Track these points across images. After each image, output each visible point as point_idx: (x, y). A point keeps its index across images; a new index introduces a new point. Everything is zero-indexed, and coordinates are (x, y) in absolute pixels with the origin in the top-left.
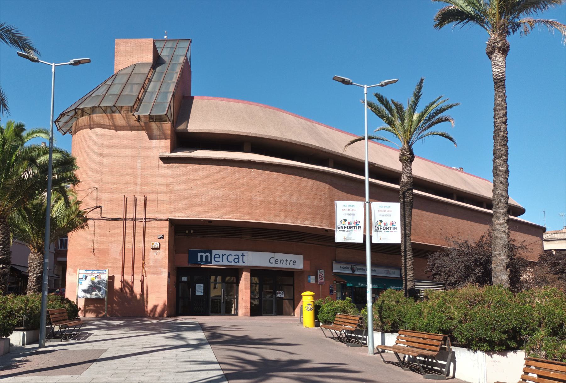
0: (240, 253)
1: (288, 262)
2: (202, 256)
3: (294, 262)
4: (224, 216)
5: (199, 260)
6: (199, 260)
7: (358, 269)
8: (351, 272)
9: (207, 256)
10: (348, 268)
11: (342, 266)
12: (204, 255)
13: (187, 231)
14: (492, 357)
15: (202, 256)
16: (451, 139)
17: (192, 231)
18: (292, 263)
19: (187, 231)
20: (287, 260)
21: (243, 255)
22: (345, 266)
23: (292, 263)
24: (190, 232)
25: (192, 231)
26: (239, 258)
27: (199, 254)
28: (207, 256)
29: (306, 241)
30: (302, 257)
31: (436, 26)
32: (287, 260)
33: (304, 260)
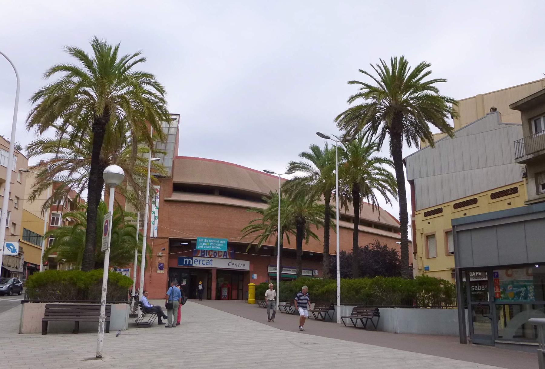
2: (186, 261)
3: (244, 265)
12: (188, 260)
15: (186, 261)
27: (185, 260)
28: (190, 261)
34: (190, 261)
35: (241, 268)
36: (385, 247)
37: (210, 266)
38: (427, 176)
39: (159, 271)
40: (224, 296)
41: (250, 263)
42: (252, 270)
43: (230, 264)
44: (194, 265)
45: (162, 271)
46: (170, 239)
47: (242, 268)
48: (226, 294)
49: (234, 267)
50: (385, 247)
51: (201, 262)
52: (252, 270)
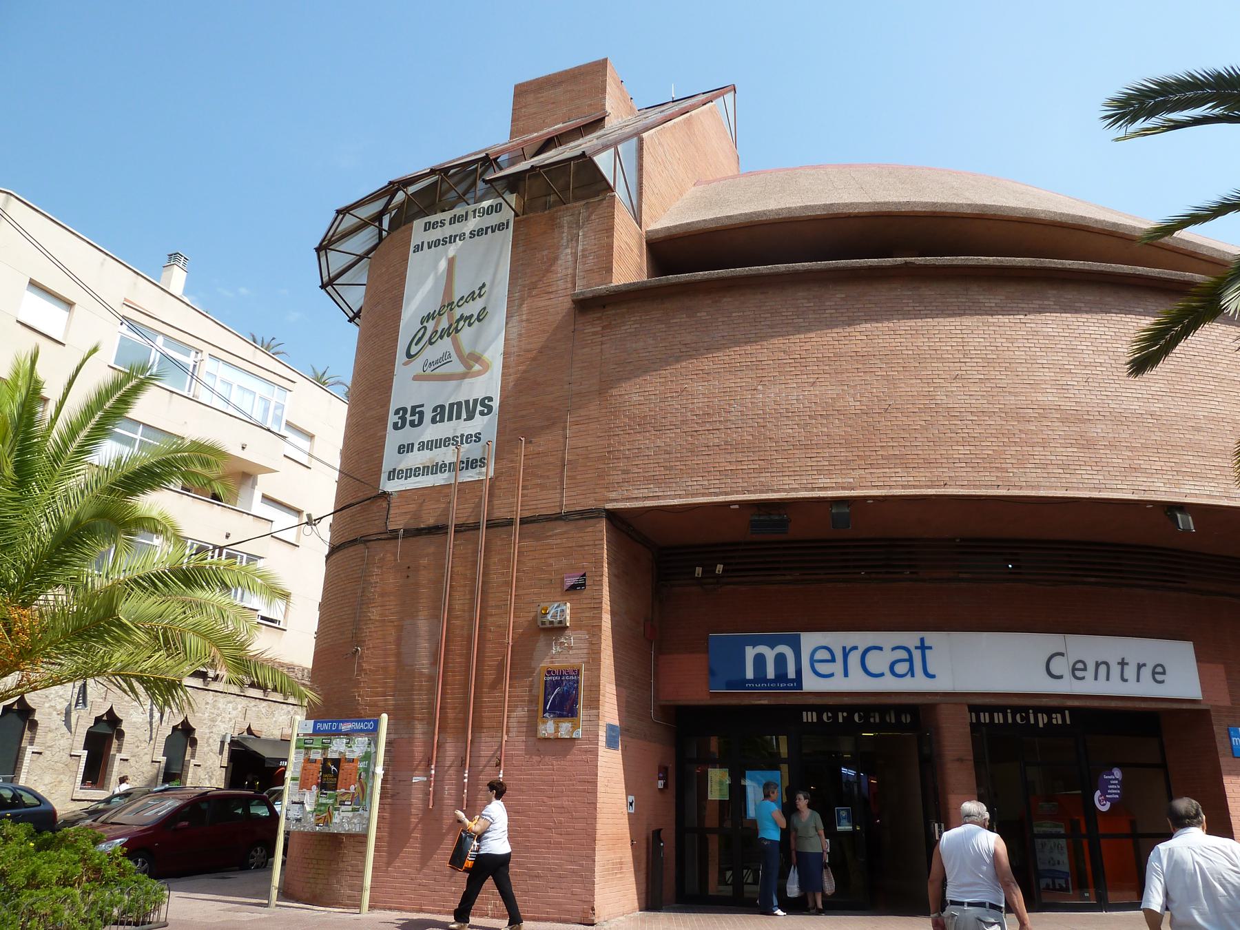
0: (910, 639)
1: (1130, 672)
2: (760, 660)
3: (1159, 672)
5: (750, 674)
6: (750, 674)
12: (770, 654)
15: (760, 660)
18: (1146, 673)
20: (1123, 663)
21: (923, 647)
23: (1146, 673)
24: (709, 571)
26: (910, 660)
27: (750, 653)
28: (780, 660)
34: (780, 660)
35: (1144, 688)
36: (423, 733)
37: (917, 684)
38: (302, 803)
39: (548, 728)
40: (1054, 875)
41: (1201, 658)
42: (1225, 701)
43: (1059, 666)
44: (811, 684)
45: (565, 729)
46: (624, 525)
47: (1145, 688)
48: (1063, 862)
49: (1090, 686)
50: (423, 733)
51: (854, 658)
52: (1225, 701)
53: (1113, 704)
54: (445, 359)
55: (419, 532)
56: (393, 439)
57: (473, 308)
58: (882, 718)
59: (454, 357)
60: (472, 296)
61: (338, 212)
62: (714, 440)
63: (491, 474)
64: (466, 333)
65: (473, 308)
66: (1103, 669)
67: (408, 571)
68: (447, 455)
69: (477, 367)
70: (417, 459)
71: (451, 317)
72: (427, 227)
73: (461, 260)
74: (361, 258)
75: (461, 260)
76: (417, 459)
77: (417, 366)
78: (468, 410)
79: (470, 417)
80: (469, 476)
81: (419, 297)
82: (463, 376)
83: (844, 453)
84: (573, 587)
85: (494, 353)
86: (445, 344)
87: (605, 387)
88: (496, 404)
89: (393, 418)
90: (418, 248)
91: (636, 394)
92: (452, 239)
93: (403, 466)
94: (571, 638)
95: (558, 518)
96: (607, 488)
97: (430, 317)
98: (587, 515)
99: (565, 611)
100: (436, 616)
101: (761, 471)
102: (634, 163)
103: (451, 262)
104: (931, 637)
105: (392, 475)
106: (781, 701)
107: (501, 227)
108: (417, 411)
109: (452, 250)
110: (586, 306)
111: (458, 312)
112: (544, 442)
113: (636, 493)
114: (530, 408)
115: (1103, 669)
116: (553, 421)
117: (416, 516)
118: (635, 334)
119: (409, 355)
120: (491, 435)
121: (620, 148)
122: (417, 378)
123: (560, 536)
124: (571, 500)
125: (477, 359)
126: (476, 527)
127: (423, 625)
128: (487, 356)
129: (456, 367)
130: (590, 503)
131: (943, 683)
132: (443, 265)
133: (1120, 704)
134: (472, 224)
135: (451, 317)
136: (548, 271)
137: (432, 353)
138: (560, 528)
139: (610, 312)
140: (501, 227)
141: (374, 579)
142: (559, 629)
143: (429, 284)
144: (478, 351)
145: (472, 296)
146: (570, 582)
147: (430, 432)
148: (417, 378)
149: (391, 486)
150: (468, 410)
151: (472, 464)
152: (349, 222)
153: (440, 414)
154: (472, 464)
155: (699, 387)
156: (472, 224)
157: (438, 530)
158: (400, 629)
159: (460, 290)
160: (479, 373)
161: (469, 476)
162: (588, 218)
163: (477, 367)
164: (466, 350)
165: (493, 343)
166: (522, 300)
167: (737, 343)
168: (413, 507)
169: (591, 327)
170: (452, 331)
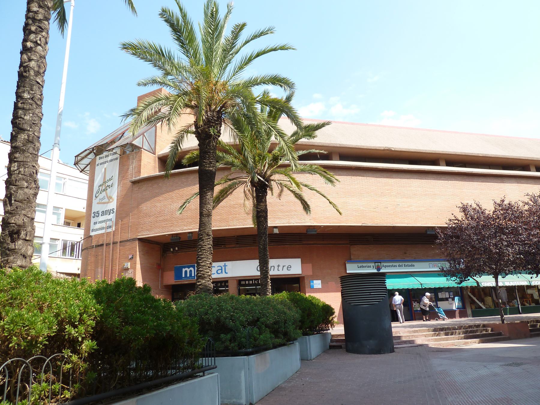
0: (222, 264)
1: (280, 268)
2: (186, 272)
3: (289, 267)
4: (185, 228)
5: (183, 276)
6: (183, 276)
7: (385, 267)
8: (375, 271)
9: (191, 271)
10: (369, 267)
11: (360, 265)
12: (188, 270)
13: (172, 249)
14: (464, 209)
15: (186, 272)
16: (282, 48)
17: (177, 248)
18: (285, 268)
19: (172, 249)
20: (279, 266)
21: (225, 266)
22: (364, 265)
23: (285, 268)
24: (174, 249)
25: (177, 248)
26: (222, 269)
27: (184, 270)
28: (191, 271)
29: (304, 242)
30: (299, 261)
31: (164, 11)
32: (279, 266)
33: (302, 263)
52: (310, 272)
53: (275, 277)
54: (103, 198)
55: (99, 246)
56: (93, 220)
57: (109, 183)
58: (221, 284)
59: (106, 197)
60: (110, 180)
61: (76, 157)
62: (161, 218)
63: (114, 229)
64: (109, 190)
65: (109, 183)
66: (273, 268)
67: (96, 256)
68: (104, 225)
69: (111, 200)
70: (98, 226)
71: (105, 186)
72: (100, 158)
73: (108, 168)
74: (88, 165)
75: (108, 168)
76: (98, 226)
77: (97, 200)
78: (108, 212)
79: (109, 214)
80: (109, 230)
81: (98, 180)
82: (108, 203)
83: (190, 220)
84: (130, 259)
85: (115, 197)
86: (104, 194)
87: (139, 204)
88: (115, 210)
89: (93, 215)
90: (98, 165)
91: (146, 207)
92: (105, 163)
93: (95, 228)
94: (130, 271)
95: (128, 241)
96: (139, 232)
97: (100, 186)
98: (134, 240)
99: (128, 265)
100: (102, 268)
101: (171, 226)
102: (272, 45)
103: (105, 169)
104: (227, 263)
105: (93, 230)
106: (191, 282)
107: (116, 159)
108: (98, 213)
109: (105, 165)
110: (134, 183)
111: (107, 184)
112: (125, 221)
113: (144, 234)
114: (123, 212)
115: (273, 268)
116: (127, 215)
117: (98, 242)
118: (145, 189)
119: (96, 197)
120: (114, 220)
121: (145, 134)
122: (98, 203)
123: (128, 245)
124: (130, 236)
125: (111, 198)
126: (110, 244)
127: (99, 270)
128: (113, 197)
129: (106, 200)
130: (134, 237)
131: (229, 275)
132: (103, 170)
133: (284, 277)
134: (110, 158)
135: (105, 186)
136: (127, 172)
137: (101, 196)
138: (128, 243)
139: (140, 184)
140: (116, 159)
141: (89, 259)
142: (127, 269)
143: (100, 176)
144: (111, 195)
145: (110, 180)
146: (130, 257)
147: (101, 218)
148: (98, 203)
149: (92, 234)
150: (108, 212)
151: (110, 227)
152: (79, 158)
153: (104, 213)
154: (110, 227)
155: (158, 205)
156: (110, 158)
157: (102, 245)
158: (95, 271)
159: (107, 178)
160: (111, 202)
161: (109, 230)
162: (136, 157)
163: (111, 200)
164: (109, 196)
165: (114, 193)
166: (121, 180)
167: (168, 192)
168: (97, 239)
169: (136, 188)
170: (105, 190)
